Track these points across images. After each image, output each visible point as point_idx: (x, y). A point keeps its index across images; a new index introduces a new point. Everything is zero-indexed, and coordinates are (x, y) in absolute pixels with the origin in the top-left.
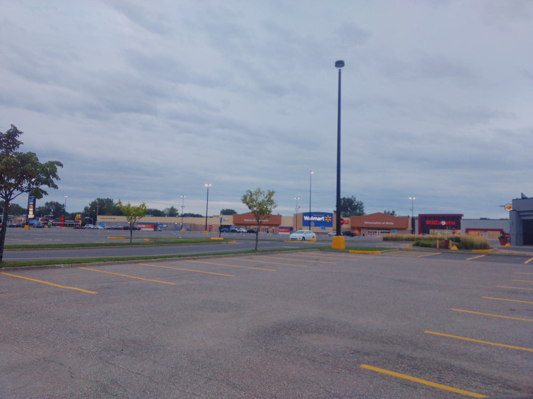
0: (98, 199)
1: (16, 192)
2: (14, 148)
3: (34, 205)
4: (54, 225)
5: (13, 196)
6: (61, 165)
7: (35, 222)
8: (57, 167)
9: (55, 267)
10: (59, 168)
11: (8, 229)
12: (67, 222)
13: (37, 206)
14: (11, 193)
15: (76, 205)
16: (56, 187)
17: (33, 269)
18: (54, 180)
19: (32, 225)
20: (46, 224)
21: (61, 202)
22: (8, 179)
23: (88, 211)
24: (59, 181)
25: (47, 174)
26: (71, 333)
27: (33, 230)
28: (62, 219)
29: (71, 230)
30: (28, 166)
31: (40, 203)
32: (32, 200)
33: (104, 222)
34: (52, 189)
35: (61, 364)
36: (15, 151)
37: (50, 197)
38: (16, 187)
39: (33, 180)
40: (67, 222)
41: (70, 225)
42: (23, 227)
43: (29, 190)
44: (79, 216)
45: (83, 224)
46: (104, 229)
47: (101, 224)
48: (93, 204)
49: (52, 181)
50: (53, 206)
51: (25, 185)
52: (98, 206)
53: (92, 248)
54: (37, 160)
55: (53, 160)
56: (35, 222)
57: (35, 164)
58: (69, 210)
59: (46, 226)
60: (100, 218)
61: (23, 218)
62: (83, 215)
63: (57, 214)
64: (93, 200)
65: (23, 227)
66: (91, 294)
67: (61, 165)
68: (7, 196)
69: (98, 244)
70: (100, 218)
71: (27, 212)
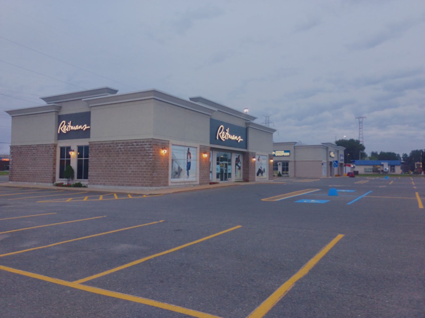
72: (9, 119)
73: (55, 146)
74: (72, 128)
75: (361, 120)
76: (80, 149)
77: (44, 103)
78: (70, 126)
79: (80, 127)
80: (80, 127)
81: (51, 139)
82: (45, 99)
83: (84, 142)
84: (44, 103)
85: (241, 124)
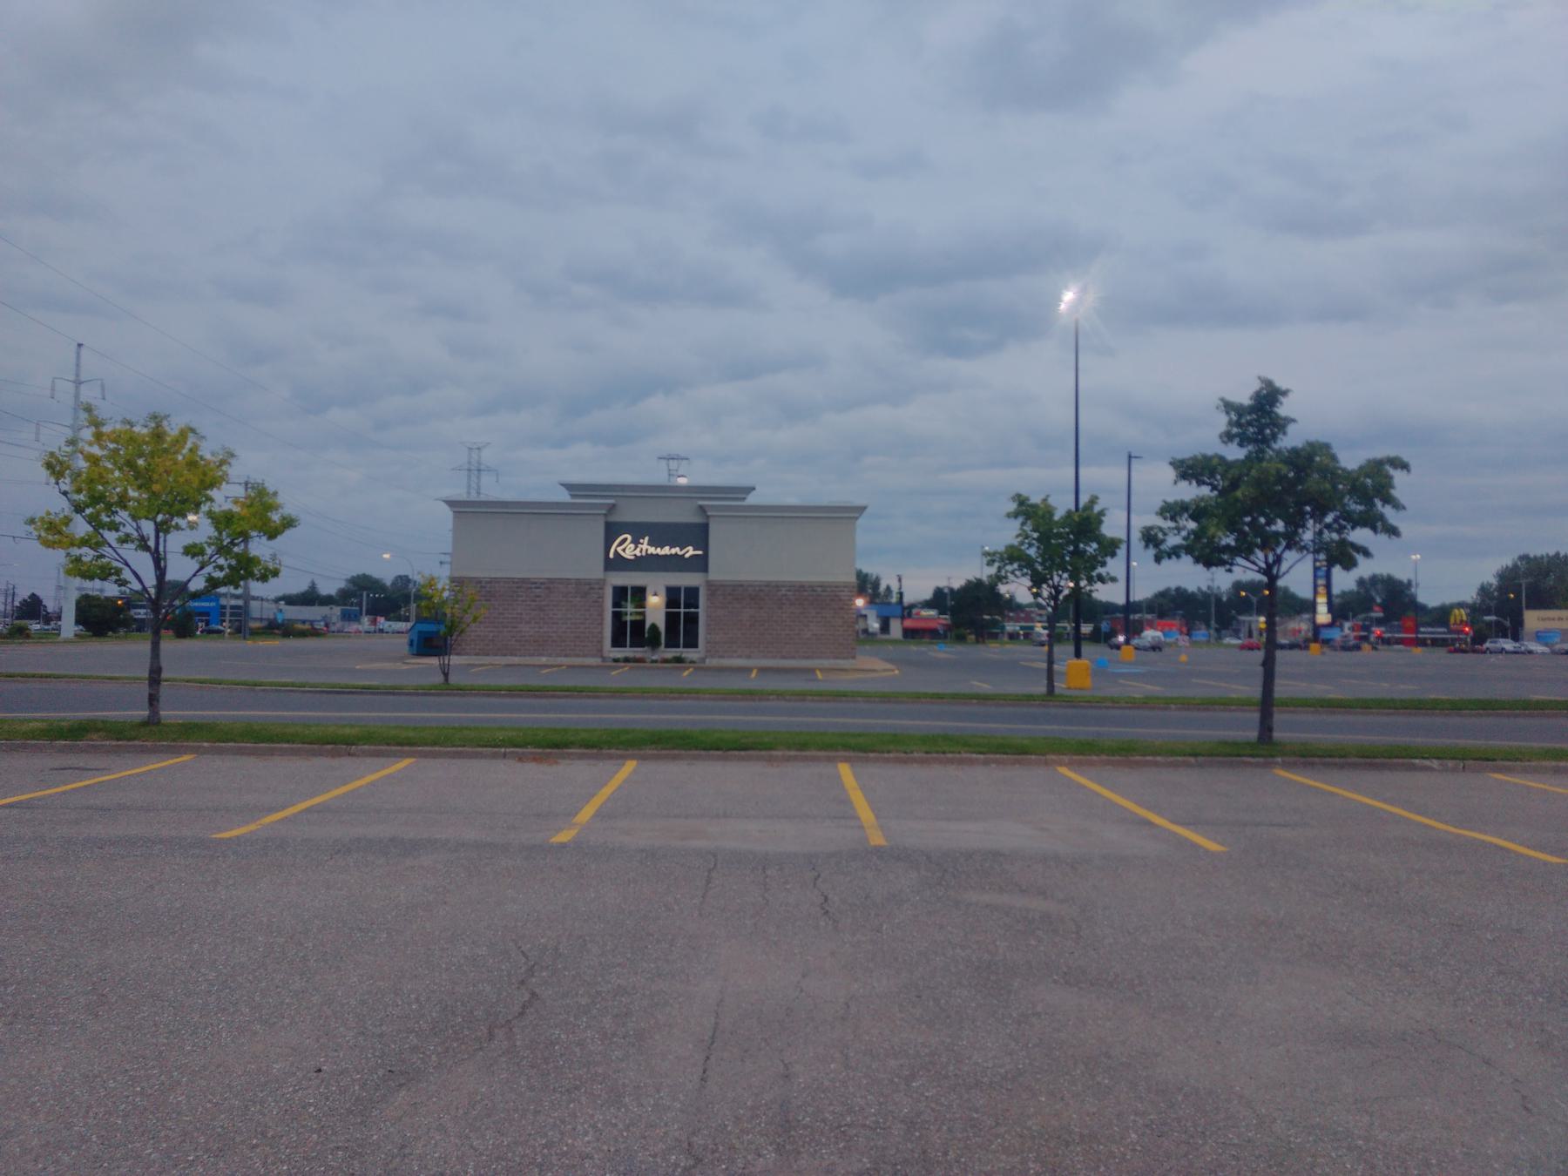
0: (1525, 558)
1: (1290, 556)
2: (1274, 437)
3: (1328, 586)
4: (1387, 642)
5: (1284, 566)
6: (1404, 466)
7: (1335, 634)
8: (1392, 471)
9: (1413, 768)
10: (1398, 476)
11: (1279, 654)
12: (1426, 632)
13: (1336, 591)
14: (1278, 560)
15: (1449, 577)
16: (1393, 531)
17: (1355, 766)
18: (1388, 511)
19: (1326, 642)
20: (1365, 639)
21: (1402, 575)
22: (1269, 523)
23: (1492, 598)
24: (1402, 513)
25: (1366, 497)
26: (1500, 973)
27: (1331, 656)
28: (1409, 624)
29: (1441, 654)
30: (1314, 481)
31: (1344, 581)
32: (1321, 573)
33: (1548, 631)
34: (1383, 537)
35: (1487, 1062)
36: (1276, 446)
37: (1383, 559)
38: (1292, 542)
39: (1329, 519)
40: (1426, 632)
41: (1436, 643)
42: (1307, 648)
43: (1319, 547)
44: (1462, 614)
45: (1479, 638)
46: (1554, 652)
47: (1539, 637)
48: (1508, 578)
49: (1382, 517)
50: (1379, 586)
51: (1308, 536)
52: (1524, 582)
53: (1516, 716)
54: (1334, 458)
55: (1379, 453)
56: (1335, 634)
57: (1331, 472)
58: (1429, 596)
59: (1366, 646)
60: (1533, 619)
61: (1301, 625)
62: (1475, 610)
63: (1391, 607)
64: (1507, 561)
65: (1307, 648)
66: (1545, 863)
67: (1404, 466)
68: (1269, 567)
69: (1543, 702)
70: (1533, 619)
71: (1311, 607)
72: (448, 513)
73: (601, 584)
74: (652, 550)
75: (674, 465)
76: (673, 596)
77: (564, 496)
78: (645, 546)
79: (676, 550)
80: (676, 550)
81: (595, 571)
82: (569, 487)
83: (684, 580)
84: (564, 496)
85: (683, 514)
